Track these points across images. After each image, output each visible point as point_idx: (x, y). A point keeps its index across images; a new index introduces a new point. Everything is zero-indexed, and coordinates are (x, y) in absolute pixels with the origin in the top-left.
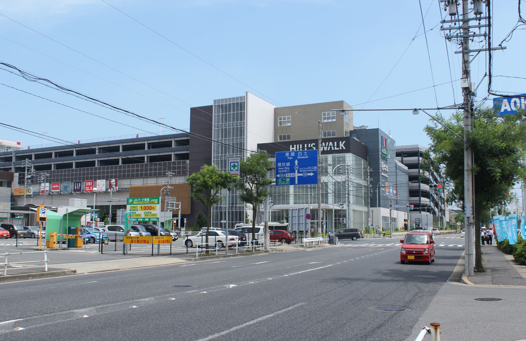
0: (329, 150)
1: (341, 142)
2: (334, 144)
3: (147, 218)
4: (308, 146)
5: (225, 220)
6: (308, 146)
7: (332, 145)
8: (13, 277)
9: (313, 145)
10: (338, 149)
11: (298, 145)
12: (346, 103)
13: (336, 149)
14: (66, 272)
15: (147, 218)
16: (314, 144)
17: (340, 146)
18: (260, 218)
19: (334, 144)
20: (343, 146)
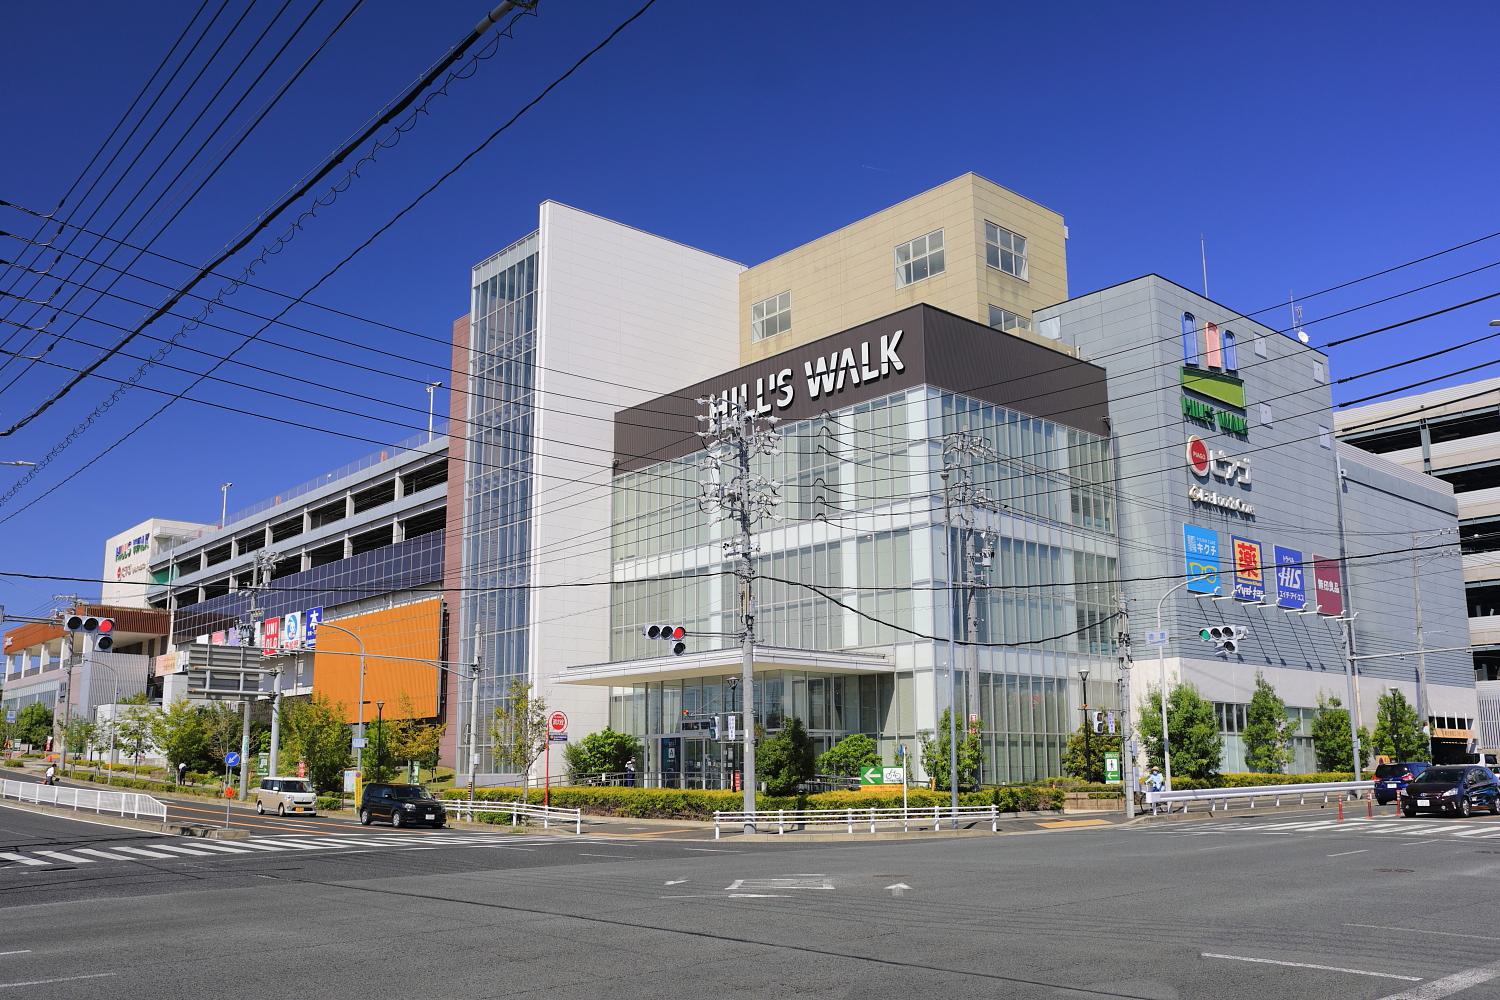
0: (834, 356)
1: (884, 339)
2: (857, 355)
3: (1186, 539)
4: (765, 384)
5: (239, 675)
6: (765, 384)
7: (851, 363)
8: (952, 540)
9: (785, 378)
10: (875, 374)
11: (734, 390)
12: (750, 843)
13: (867, 375)
14: (265, 734)
15: (1186, 539)
16: (788, 372)
17: (884, 359)
18: (500, 655)
19: (857, 355)
20: (894, 358)
